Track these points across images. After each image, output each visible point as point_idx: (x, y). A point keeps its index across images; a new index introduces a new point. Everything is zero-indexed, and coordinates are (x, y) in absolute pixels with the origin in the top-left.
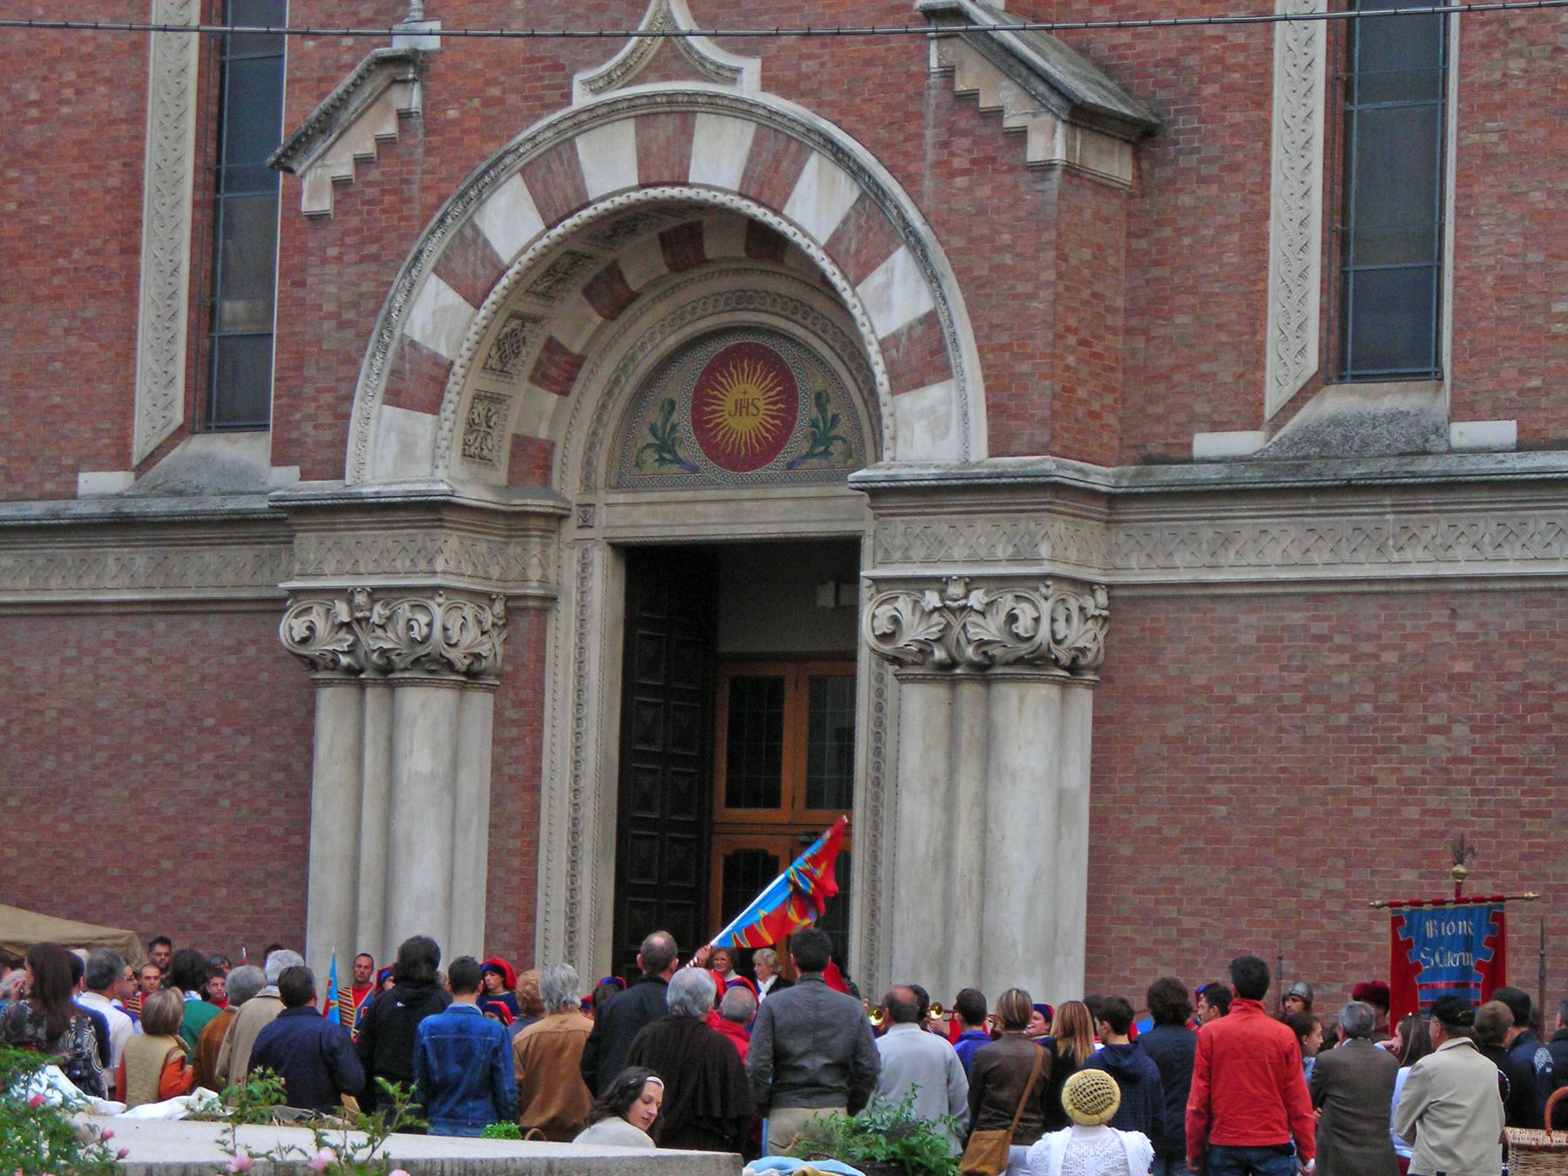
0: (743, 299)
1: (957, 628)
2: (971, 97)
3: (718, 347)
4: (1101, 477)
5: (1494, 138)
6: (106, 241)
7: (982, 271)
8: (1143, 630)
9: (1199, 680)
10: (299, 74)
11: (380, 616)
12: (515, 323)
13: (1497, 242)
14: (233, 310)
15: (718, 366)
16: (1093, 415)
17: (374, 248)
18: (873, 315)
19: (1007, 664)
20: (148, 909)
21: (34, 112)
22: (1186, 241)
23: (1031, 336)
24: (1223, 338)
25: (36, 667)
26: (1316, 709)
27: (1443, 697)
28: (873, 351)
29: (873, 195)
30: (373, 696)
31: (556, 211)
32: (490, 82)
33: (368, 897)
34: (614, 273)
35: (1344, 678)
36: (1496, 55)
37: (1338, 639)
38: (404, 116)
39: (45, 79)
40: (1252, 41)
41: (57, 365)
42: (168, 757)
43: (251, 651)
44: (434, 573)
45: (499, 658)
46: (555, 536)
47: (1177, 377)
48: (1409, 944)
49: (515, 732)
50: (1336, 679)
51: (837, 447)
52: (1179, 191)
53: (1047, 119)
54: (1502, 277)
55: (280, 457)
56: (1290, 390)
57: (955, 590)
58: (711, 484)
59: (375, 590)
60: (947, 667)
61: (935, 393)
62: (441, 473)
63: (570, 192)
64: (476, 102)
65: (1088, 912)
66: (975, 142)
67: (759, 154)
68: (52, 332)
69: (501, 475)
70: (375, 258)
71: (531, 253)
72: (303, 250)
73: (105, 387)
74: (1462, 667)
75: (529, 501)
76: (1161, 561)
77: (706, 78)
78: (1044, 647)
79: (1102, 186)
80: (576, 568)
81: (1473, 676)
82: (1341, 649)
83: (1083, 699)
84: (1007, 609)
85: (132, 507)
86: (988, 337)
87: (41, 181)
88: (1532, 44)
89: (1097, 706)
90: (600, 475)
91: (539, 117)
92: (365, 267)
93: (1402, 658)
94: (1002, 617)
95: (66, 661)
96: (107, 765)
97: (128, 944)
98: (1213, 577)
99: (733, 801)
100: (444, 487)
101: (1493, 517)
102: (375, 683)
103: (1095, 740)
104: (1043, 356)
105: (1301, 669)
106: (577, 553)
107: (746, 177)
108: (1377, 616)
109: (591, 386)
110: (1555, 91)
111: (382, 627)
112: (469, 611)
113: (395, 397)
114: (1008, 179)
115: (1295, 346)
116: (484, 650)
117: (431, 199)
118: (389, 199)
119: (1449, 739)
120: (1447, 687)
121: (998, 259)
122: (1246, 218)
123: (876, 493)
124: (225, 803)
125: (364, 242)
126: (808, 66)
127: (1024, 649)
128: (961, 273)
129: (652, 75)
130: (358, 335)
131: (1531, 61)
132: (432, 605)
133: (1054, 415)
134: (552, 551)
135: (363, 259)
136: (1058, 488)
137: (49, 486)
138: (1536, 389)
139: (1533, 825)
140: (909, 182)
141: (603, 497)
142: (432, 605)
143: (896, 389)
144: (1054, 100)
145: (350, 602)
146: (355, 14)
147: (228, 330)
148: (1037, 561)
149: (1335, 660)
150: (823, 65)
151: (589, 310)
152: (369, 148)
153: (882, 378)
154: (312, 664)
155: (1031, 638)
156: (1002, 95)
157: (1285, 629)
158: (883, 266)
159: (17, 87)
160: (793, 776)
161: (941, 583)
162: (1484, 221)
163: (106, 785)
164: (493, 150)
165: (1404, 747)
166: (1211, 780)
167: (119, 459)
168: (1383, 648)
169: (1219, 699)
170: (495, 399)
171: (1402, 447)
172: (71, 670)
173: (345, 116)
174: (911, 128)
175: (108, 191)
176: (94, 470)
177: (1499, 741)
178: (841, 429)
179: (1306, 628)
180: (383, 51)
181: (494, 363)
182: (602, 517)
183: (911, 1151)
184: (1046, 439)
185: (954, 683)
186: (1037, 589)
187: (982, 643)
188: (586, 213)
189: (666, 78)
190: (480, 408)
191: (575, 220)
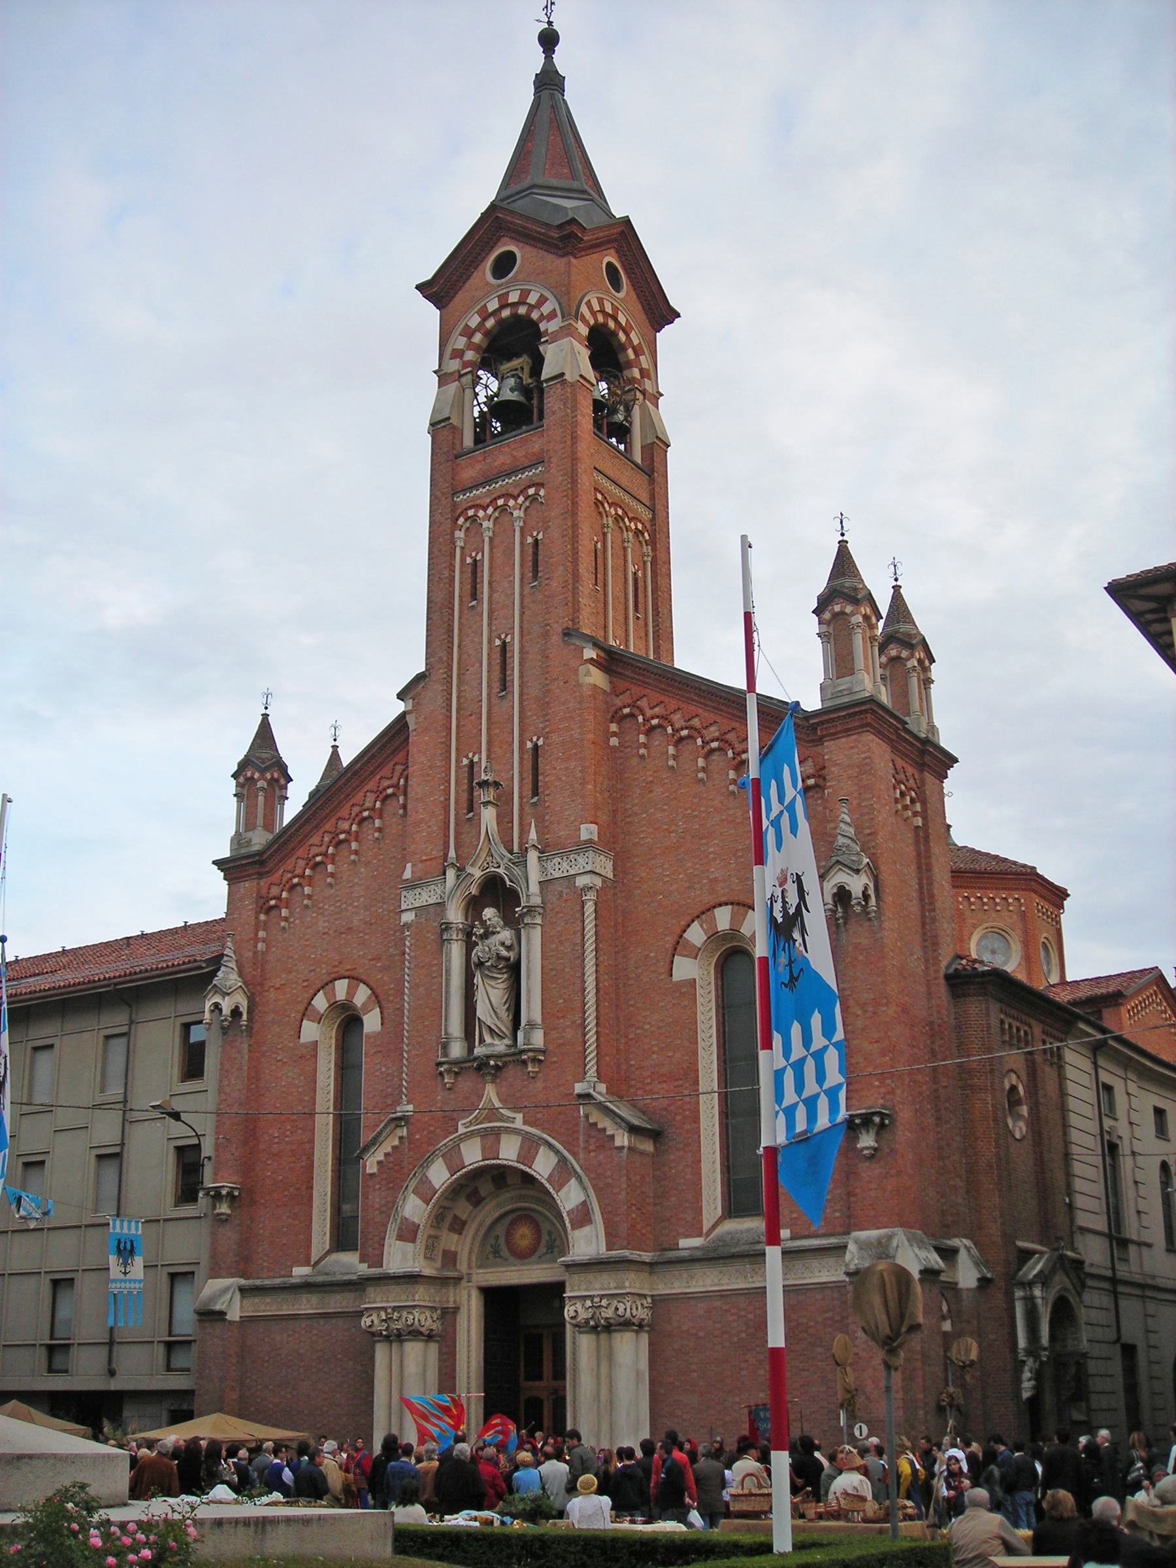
0: (521, 1198)
2: (595, 1124)
3: (514, 1215)
4: (647, 1257)
7: (601, 1185)
9: (685, 1328)
12: (441, 1210)
14: (346, 1208)
15: (513, 1223)
16: (643, 1234)
19: (616, 1325)
21: (276, 1140)
22: (673, 1171)
24: (687, 1205)
28: (565, 1215)
29: (563, 1161)
30: (394, 1345)
32: (431, 1125)
34: (476, 1191)
35: (735, 1324)
37: (732, 1311)
38: (401, 1138)
44: (415, 1301)
48: (755, 1420)
49: (446, 1357)
51: (556, 1250)
53: (622, 1131)
55: (362, 1261)
56: (712, 1222)
57: (597, 1300)
59: (395, 1307)
60: (595, 1328)
61: (587, 1230)
62: (416, 1265)
63: (459, 1163)
69: (439, 1264)
70: (393, 1188)
72: (368, 1186)
73: (301, 1237)
76: (670, 1285)
77: (504, 1121)
79: (642, 1153)
80: (466, 1297)
83: (645, 1338)
85: (310, 1280)
89: (649, 1337)
90: (474, 1264)
94: (613, 1309)
97: (308, 1438)
98: (674, 1292)
99: (528, 1379)
100: (417, 1270)
102: (395, 1341)
105: (720, 1322)
109: (470, 1231)
112: (428, 1313)
113: (400, 1237)
114: (609, 1153)
115: (713, 1207)
116: (434, 1327)
118: (397, 1168)
122: (693, 1162)
123: (568, 1266)
125: (389, 1183)
126: (539, 1116)
127: (622, 1320)
128: (594, 1187)
132: (414, 1312)
133: (628, 1235)
136: (631, 1262)
137: (282, 1273)
139: (806, 1374)
140: (574, 1155)
141: (474, 1271)
142: (414, 1312)
143: (573, 1229)
144: (623, 1124)
145: (386, 1311)
147: (344, 1215)
148: (624, 1288)
149: (731, 1318)
151: (468, 1204)
152: (389, 1150)
153: (568, 1225)
154: (373, 1334)
156: (605, 1123)
159: (271, 1131)
160: (547, 1368)
161: (591, 1297)
164: (432, 1149)
167: (307, 1262)
170: (436, 1237)
171: (751, 1240)
173: (381, 1139)
174: (575, 1136)
175: (302, 1167)
178: (557, 1243)
180: (394, 1116)
182: (475, 1278)
183: (539, 1506)
185: (598, 1333)
188: (465, 1170)
189: (490, 1122)
191: (460, 1173)
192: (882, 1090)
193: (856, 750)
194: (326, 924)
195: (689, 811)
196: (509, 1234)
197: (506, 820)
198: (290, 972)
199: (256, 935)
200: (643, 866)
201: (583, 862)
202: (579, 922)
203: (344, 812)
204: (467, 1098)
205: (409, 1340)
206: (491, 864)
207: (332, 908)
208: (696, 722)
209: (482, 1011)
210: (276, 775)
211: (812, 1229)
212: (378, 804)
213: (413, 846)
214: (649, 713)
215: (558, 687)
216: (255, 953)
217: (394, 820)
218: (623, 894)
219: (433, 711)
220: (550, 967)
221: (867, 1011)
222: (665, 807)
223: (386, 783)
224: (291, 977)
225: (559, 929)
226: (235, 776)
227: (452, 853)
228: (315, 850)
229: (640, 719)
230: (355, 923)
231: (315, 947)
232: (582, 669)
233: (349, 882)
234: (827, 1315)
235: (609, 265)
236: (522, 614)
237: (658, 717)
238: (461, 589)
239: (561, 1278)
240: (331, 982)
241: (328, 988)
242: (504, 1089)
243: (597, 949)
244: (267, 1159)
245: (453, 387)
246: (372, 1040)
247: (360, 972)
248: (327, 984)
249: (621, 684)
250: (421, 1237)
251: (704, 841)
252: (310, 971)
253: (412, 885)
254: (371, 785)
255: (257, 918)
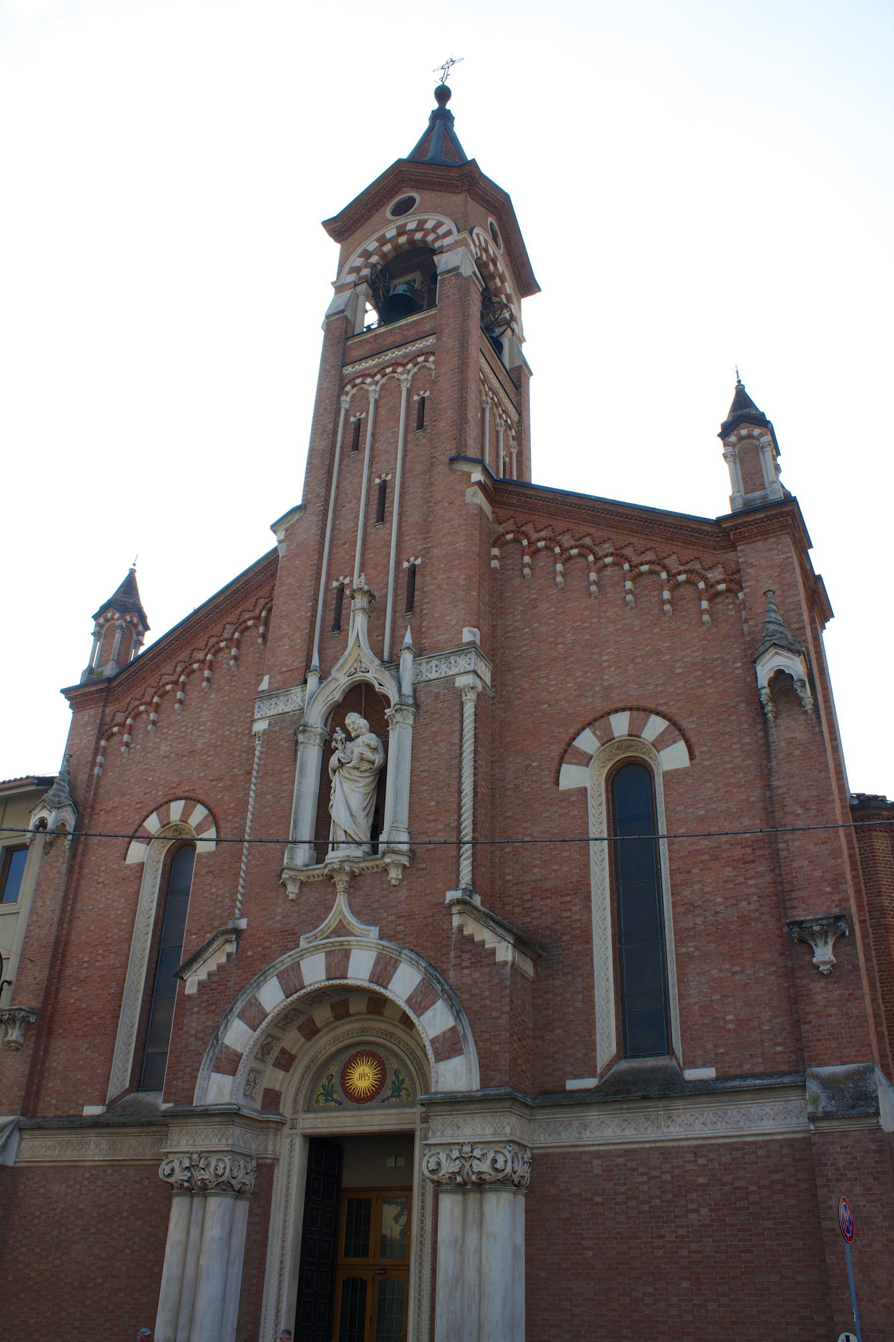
1: (467, 1167)
5: (692, 949)
6: (106, 1014)
8: (547, 1168)
9: (576, 1190)
10: (188, 948)
11: (203, 1165)
12: (269, 1040)
13: (698, 992)
16: (523, 1071)
17: (213, 1008)
18: (427, 1029)
20: (88, 1302)
21: (85, 965)
23: (499, 1035)
24: (577, 1038)
25: (55, 1189)
26: (632, 1203)
27: (694, 1195)
28: (428, 1044)
31: (290, 990)
33: (186, 1297)
35: (646, 1187)
36: (690, 916)
37: (641, 1170)
39: (91, 953)
40: (583, 918)
41: (81, 1062)
42: (105, 1230)
43: (146, 1182)
45: (253, 1185)
46: (280, 1132)
47: (557, 1056)
49: (257, 1219)
50: (641, 1188)
51: (403, 1093)
52: (553, 979)
53: (505, 944)
54: (702, 1006)
57: (467, 1149)
58: (347, 1109)
63: (297, 983)
64: (260, 949)
65: (526, 1306)
66: (472, 955)
67: (378, 964)
68: (81, 1050)
69: (258, 1105)
70: (214, 1011)
71: (278, 1008)
73: (99, 1071)
74: (701, 1180)
75: (270, 1116)
78: (509, 1175)
80: (288, 1146)
81: (708, 1185)
82: (643, 1174)
83: (522, 1200)
84: (491, 1157)
86: (480, 1036)
87: (85, 991)
88: (705, 911)
90: (300, 1107)
91: (286, 953)
92: (208, 1015)
93: (673, 1177)
94: (489, 1162)
95: (69, 1187)
96: (79, 1233)
101: (711, 1110)
102: (199, 1195)
103: (526, 1220)
104: (505, 1043)
105: (625, 1184)
106: (289, 1141)
107: (373, 974)
108: (659, 1158)
109: (298, 1068)
110: (718, 929)
111: (203, 1169)
114: (487, 969)
117: (238, 987)
119: (699, 1216)
120: (696, 1191)
121: (483, 1003)
124: (128, 1252)
125: (209, 1005)
126: (399, 928)
129: (333, 935)
130: (204, 1043)
131: (705, 917)
134: (278, 1139)
135: (208, 1012)
138: (723, 1053)
146: (212, 925)
150: (406, 927)
151: (300, 1036)
155: (504, 1170)
157: (616, 1166)
158: (432, 1008)
162: (691, 984)
163: (78, 1243)
165: (677, 1220)
166: (584, 1239)
167: (102, 1102)
168: (663, 1173)
169: (586, 1200)
172: (70, 1191)
176: (90, 1105)
177: (724, 1215)
179: (625, 1165)
181: (259, 1056)
184: (507, 1079)
185: (465, 1193)
186: (505, 1147)
187: (480, 1173)
189: (339, 936)
190: (252, 1075)
192: (836, 897)
193: (776, 552)
194: (168, 748)
195: (579, 624)
196: (344, 1074)
197: (376, 633)
198: (124, 795)
199: (94, 759)
200: (525, 677)
201: (463, 663)
202: (457, 722)
203: (201, 643)
204: (312, 910)
205: (216, 1195)
206: (358, 669)
207: (177, 733)
208: (587, 541)
209: (338, 811)
210: (135, 620)
211: (747, 1067)
212: (237, 635)
213: (272, 660)
214: (534, 536)
215: (443, 508)
216: (91, 776)
217: (252, 649)
218: (502, 706)
219: (306, 539)
220: (422, 768)
221: (809, 810)
222: (551, 621)
223: (247, 616)
224: (125, 799)
225: (434, 729)
226: (96, 617)
227: (315, 661)
228: (166, 678)
229: (525, 542)
230: (199, 745)
231: (153, 770)
232: (469, 491)
233: (198, 707)
234: (776, 1177)
235: (491, 223)
236: (405, 456)
237: (544, 539)
238: (343, 441)
239: (409, 1126)
240: (166, 803)
241: (162, 809)
242: (358, 900)
243: (475, 752)
244: (73, 985)
245: (347, 294)
246: (204, 860)
247: (200, 793)
248: (161, 805)
249: (502, 512)
250: (243, 1068)
251: (596, 650)
252: (145, 794)
253: (270, 695)
254: (232, 618)
255: (97, 743)
